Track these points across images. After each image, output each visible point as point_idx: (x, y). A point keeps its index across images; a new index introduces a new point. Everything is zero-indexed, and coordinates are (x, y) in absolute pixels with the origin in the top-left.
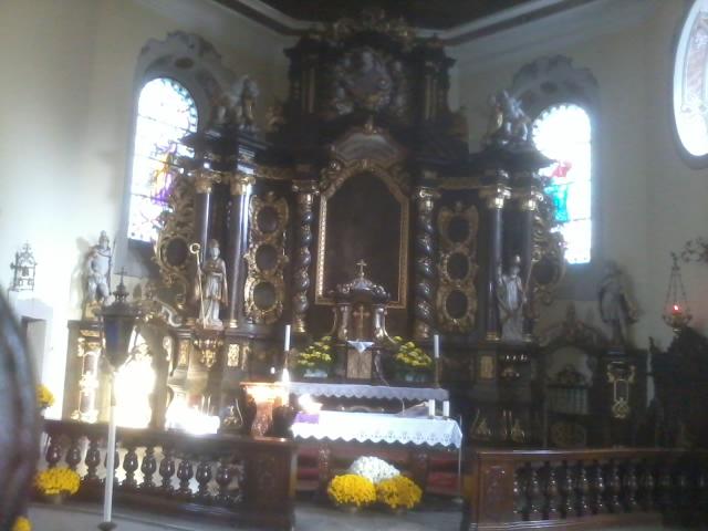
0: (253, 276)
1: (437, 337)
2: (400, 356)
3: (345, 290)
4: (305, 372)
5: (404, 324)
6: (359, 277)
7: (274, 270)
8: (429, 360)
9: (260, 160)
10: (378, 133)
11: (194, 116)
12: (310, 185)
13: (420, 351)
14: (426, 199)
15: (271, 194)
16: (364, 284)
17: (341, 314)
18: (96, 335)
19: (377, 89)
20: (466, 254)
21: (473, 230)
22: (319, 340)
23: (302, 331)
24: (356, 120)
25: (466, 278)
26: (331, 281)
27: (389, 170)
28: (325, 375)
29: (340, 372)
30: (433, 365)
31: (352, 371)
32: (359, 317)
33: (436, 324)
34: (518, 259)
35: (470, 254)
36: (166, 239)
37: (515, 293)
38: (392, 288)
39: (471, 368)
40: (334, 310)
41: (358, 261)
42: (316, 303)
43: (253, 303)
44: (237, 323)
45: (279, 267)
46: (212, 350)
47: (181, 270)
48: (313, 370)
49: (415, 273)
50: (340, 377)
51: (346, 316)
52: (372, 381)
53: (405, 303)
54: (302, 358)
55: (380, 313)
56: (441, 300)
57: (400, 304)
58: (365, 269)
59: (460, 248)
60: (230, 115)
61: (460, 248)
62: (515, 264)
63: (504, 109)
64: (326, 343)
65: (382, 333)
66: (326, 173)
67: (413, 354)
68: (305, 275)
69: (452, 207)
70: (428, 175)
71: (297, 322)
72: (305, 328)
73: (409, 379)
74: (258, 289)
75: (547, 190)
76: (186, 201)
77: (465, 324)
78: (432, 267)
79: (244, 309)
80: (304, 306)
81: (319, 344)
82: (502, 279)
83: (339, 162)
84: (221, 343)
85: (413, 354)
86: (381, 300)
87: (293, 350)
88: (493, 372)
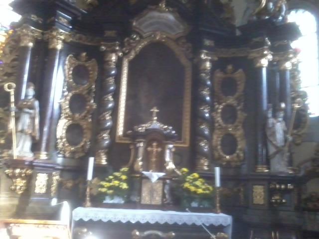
0: (66, 118)
1: (217, 170)
2: (187, 185)
3: (141, 129)
4: (104, 199)
5: (189, 158)
6: (153, 120)
7: (83, 114)
8: (211, 188)
10: (169, 12)
12: (115, 45)
13: (203, 181)
14: (206, 60)
15: (84, 54)
16: (156, 124)
17: (137, 149)
18: (166, 202)
20: (235, 105)
22: (118, 171)
25: (236, 124)
27: (177, 40)
28: (123, 202)
29: (135, 199)
30: (214, 192)
31: (146, 198)
33: (215, 161)
35: (239, 104)
38: (178, 127)
39: (242, 195)
40: (132, 147)
44: (47, 155)
45: (88, 112)
46: (23, 179)
48: (112, 196)
49: (196, 117)
50: (135, 203)
51: (141, 151)
52: (163, 207)
54: (102, 187)
55: (170, 149)
56: (217, 139)
57: (184, 143)
58: (158, 114)
59: (231, 100)
61: (231, 100)
64: (124, 173)
65: (171, 166)
66: (128, 40)
67: (198, 183)
68: (108, 117)
69: (223, 70)
70: (208, 42)
71: (99, 156)
72: (107, 161)
73: (194, 204)
74: (70, 129)
75: (294, 60)
76: (13, 57)
79: (56, 144)
80: (107, 142)
81: (117, 174)
83: (138, 33)
84: (29, 172)
85: (198, 183)
86: (169, 138)
87: (96, 179)
88: (264, 199)
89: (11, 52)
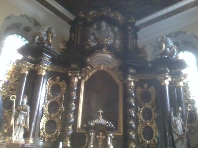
0: (46, 116)
3: (92, 124)
7: (56, 114)
9: (54, 61)
10: (109, 53)
11: (25, 41)
12: (77, 73)
14: (131, 81)
15: (58, 78)
16: (102, 121)
19: (108, 36)
21: (153, 97)
23: (69, 145)
24: (99, 48)
25: (151, 120)
26: (84, 120)
27: (113, 69)
32: (100, 138)
34: (180, 109)
35: (153, 108)
36: (4, 96)
37: (181, 126)
38: (115, 123)
40: (86, 135)
41: (99, 110)
42: (77, 131)
43: (44, 130)
44: (33, 140)
45: (60, 113)
47: (9, 112)
49: (127, 116)
51: (92, 138)
53: (122, 132)
55: (111, 137)
56: (140, 130)
57: (120, 132)
59: (148, 105)
60: (41, 39)
61: (148, 105)
62: (179, 111)
63: (166, 43)
66: (84, 70)
68: (72, 116)
69: (142, 86)
70: (132, 71)
71: (66, 141)
72: (70, 144)
75: (185, 81)
77: (153, 143)
78: (135, 113)
79: (39, 133)
82: (174, 118)
83: (90, 66)
86: (110, 129)
89: (15, 76)
